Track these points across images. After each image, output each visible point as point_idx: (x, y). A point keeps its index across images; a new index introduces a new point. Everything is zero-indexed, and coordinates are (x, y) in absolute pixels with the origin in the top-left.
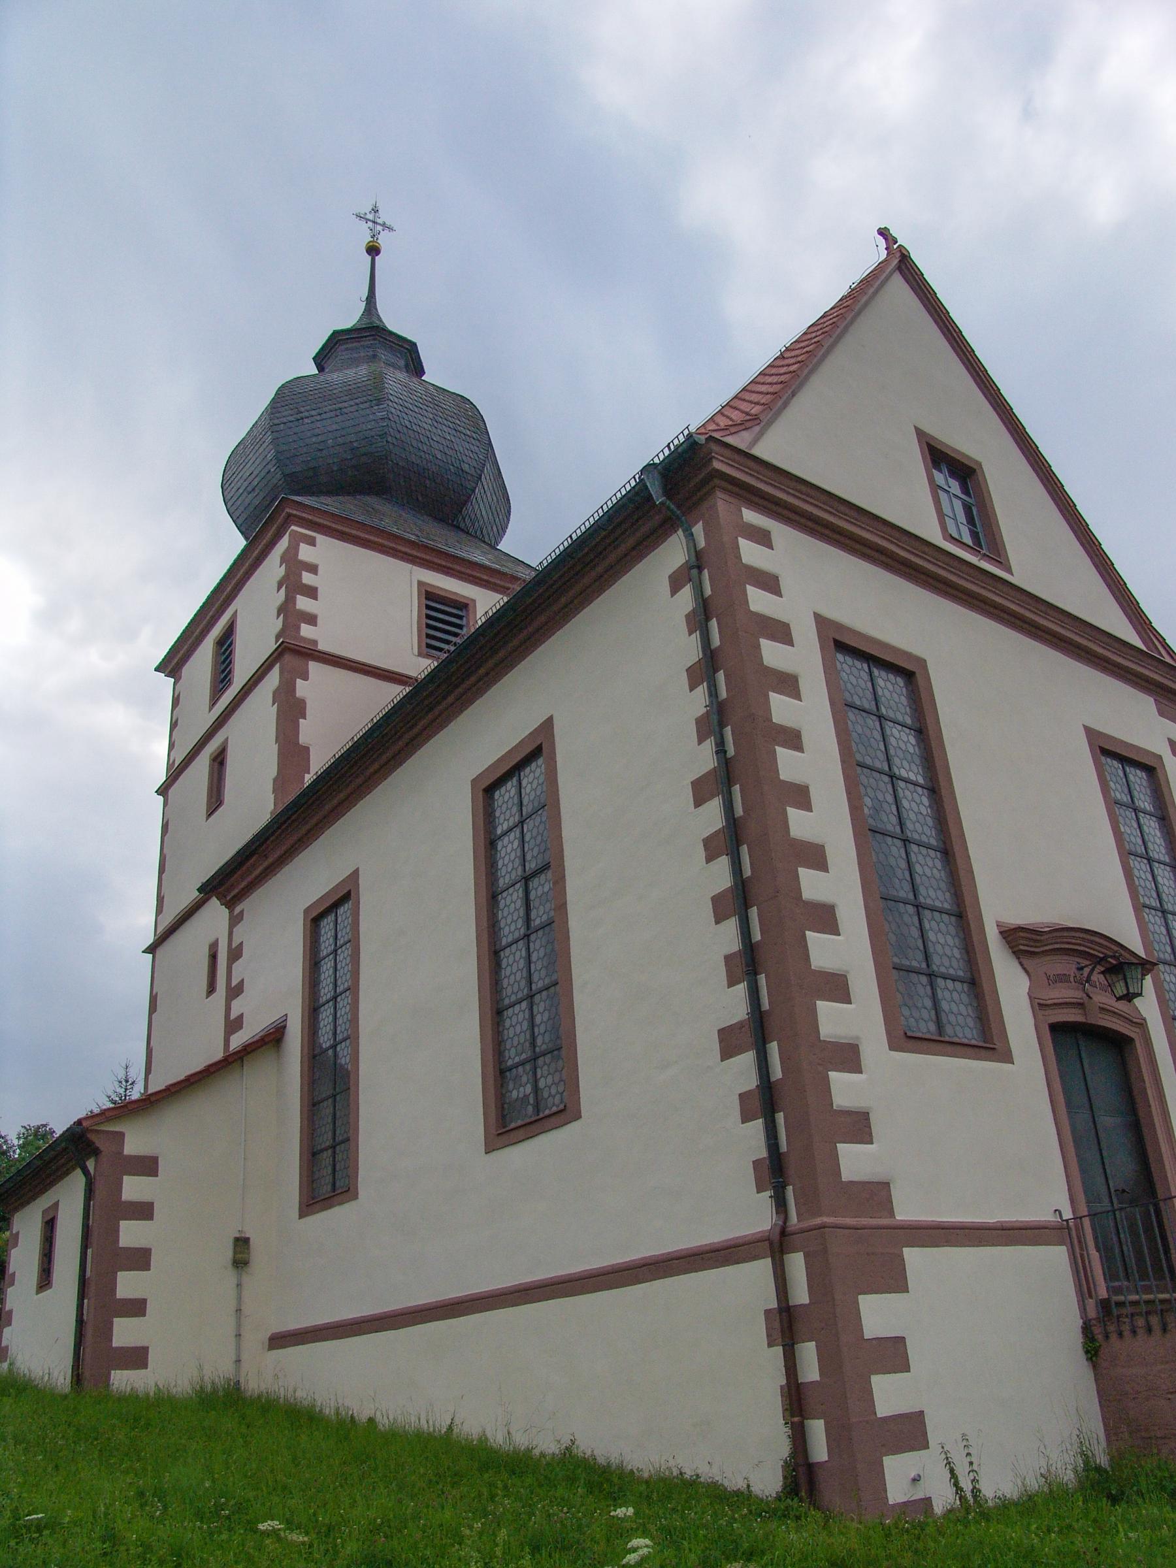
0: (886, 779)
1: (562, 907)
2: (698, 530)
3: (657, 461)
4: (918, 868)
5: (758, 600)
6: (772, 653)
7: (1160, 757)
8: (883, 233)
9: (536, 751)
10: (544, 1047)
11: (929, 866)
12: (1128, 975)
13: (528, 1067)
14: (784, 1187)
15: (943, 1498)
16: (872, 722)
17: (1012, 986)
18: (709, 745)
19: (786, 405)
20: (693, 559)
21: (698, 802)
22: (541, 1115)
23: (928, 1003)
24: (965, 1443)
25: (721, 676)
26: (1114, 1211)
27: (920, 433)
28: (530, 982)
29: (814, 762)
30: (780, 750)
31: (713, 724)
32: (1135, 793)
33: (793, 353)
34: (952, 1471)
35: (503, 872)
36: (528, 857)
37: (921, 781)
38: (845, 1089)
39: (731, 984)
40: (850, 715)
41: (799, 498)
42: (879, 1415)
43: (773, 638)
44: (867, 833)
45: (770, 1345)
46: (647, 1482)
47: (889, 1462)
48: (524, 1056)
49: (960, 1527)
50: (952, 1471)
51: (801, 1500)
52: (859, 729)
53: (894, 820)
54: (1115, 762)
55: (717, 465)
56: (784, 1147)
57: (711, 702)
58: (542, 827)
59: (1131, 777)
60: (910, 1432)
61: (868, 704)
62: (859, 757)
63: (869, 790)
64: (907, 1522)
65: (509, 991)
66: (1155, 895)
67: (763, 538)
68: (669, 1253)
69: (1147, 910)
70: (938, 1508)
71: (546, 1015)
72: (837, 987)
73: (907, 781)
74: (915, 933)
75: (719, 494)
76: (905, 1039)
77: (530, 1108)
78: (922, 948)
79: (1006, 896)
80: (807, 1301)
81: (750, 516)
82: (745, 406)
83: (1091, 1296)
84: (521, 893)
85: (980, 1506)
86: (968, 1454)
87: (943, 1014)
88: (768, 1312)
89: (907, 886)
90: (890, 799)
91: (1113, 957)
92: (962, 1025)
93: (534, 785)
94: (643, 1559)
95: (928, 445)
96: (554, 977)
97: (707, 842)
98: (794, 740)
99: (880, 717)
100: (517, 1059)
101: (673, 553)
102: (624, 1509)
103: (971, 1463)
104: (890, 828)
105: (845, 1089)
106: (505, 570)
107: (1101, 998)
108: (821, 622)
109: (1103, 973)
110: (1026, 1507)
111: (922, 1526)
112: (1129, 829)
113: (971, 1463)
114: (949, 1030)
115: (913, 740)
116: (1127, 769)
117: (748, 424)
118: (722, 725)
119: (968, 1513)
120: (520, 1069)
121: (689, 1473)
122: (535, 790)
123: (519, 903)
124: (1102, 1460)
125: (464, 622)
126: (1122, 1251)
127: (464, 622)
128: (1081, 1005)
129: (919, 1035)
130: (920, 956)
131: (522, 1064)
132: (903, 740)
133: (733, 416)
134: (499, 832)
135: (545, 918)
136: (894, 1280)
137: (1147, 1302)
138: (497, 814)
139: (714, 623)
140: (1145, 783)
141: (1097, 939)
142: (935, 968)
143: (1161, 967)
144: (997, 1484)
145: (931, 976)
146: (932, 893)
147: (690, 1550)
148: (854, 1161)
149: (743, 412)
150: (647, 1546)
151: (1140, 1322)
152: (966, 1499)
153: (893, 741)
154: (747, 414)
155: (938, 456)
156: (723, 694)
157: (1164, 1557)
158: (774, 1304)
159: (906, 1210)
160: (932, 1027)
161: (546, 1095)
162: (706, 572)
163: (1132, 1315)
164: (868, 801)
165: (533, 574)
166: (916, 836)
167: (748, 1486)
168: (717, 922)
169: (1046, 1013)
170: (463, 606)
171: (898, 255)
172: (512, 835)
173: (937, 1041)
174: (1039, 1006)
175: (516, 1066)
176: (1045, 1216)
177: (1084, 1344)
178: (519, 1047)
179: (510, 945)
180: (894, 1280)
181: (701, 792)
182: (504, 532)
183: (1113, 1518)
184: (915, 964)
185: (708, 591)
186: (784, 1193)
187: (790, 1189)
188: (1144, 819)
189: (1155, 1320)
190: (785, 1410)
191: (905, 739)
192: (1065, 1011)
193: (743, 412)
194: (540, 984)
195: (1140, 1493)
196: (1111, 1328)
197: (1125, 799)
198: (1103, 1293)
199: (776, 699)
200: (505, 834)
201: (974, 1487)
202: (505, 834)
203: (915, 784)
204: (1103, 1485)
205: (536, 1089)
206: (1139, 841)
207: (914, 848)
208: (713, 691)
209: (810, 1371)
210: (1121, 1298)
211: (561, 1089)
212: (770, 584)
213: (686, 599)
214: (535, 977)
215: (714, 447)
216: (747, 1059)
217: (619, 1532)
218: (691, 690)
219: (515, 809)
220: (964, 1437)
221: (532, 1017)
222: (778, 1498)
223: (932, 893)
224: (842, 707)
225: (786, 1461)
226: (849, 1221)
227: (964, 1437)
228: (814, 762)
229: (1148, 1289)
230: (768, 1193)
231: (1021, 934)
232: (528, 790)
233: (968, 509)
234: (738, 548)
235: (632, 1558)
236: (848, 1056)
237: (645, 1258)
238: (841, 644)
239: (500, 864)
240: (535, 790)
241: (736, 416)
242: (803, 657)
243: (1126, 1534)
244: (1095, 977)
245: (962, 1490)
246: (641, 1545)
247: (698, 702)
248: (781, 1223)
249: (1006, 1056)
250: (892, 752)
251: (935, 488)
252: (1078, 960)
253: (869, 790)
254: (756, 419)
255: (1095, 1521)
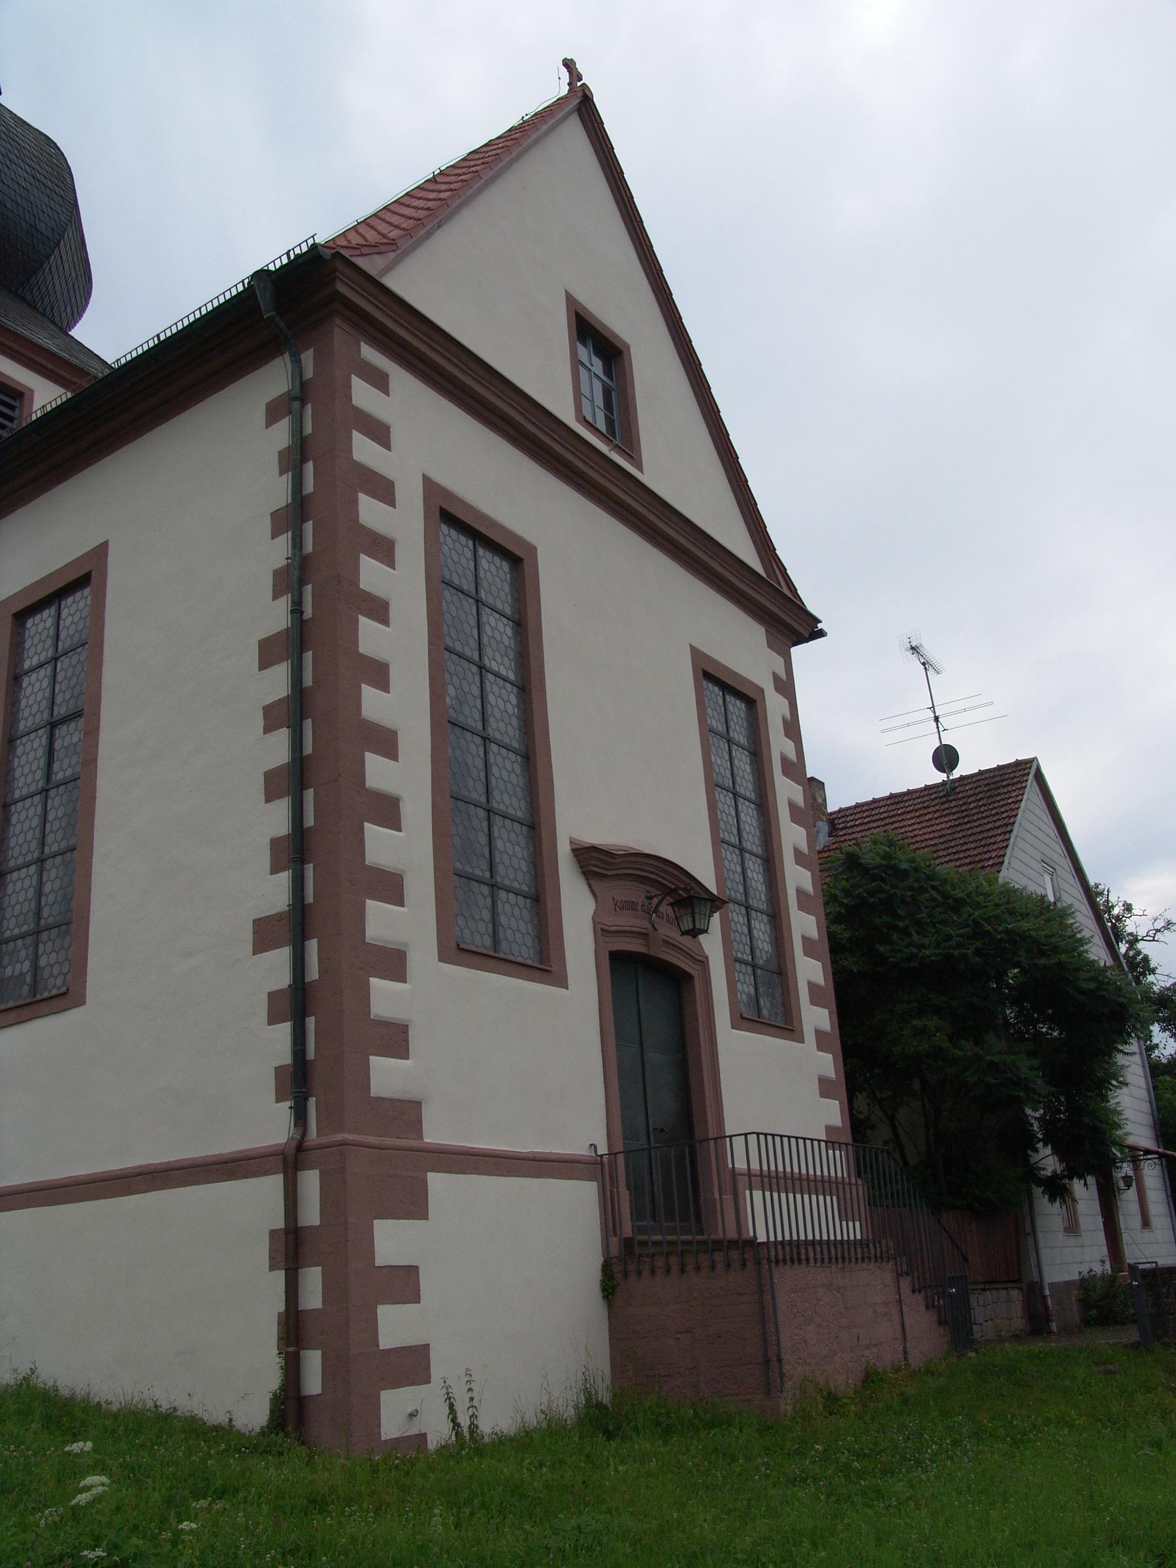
0: (475, 669)
1: (91, 762)
2: (308, 357)
3: (272, 268)
4: (495, 770)
5: (364, 449)
6: (370, 511)
7: (762, 691)
8: (569, 64)
9: (82, 579)
10: (51, 920)
11: (507, 769)
12: (697, 910)
13: (29, 940)
14: (306, 1099)
15: (438, 1432)
16: (470, 606)
17: (577, 907)
18: (284, 604)
19: (429, 235)
20: (297, 389)
21: (264, 664)
22: (38, 997)
23: (486, 915)
24: (468, 1378)
25: (309, 527)
26: (649, 1150)
27: (570, 300)
28: (43, 844)
29: (399, 639)
30: (363, 620)
31: (293, 579)
32: (732, 724)
33: (447, 179)
34: (451, 1407)
35: (26, 713)
36: (59, 699)
37: (512, 676)
38: (386, 997)
39: (275, 870)
40: (446, 592)
41: (425, 343)
42: (381, 1347)
43: (373, 494)
44: (445, 724)
45: (272, 1267)
46: (116, 1416)
47: (387, 1397)
48: (25, 928)
49: (452, 1463)
50: (451, 1407)
51: (287, 1435)
52: (454, 612)
53: (477, 715)
54: (716, 689)
55: (341, 288)
56: (311, 1054)
57: (294, 554)
58: (78, 669)
59: (730, 707)
60: (412, 1365)
61: (468, 586)
62: (449, 642)
63: (455, 679)
64: (397, 1458)
65: (16, 852)
66: (735, 832)
67: (380, 381)
68: (169, 1163)
69: (726, 846)
70: (432, 1444)
71: (57, 883)
72: (391, 887)
73: (497, 675)
74: (483, 840)
75: (338, 321)
76: (456, 951)
77: (26, 989)
78: (487, 856)
79: (587, 812)
80: (316, 1222)
81: (369, 353)
82: (383, 227)
83: (615, 1234)
84: (44, 741)
85: (476, 1442)
86: (470, 1390)
87: (501, 930)
88: (273, 1233)
89: (481, 788)
90: (476, 691)
91: (684, 890)
92: (521, 945)
93: (76, 619)
94: (98, 1499)
95: (578, 315)
96: (72, 842)
97: (268, 711)
98: (379, 610)
99: (478, 601)
100: (16, 931)
101: (273, 380)
102: (81, 1444)
103: (472, 1399)
104: (471, 722)
105: (386, 997)
106: (76, 362)
107: (668, 931)
108: (429, 485)
109: (672, 905)
110: (522, 1443)
111: (413, 1463)
112: (720, 761)
113: (472, 1399)
114: (504, 946)
115: (509, 632)
116: (728, 697)
117: (383, 249)
118: (302, 582)
119: (462, 1449)
120: (20, 942)
121: (165, 1406)
122: (76, 624)
123: (40, 752)
124: (605, 1397)
125: (16, 414)
126: (653, 1191)
127: (16, 414)
128: (644, 936)
129: (474, 948)
130: (485, 865)
131: (23, 936)
132: (499, 631)
133: (368, 236)
134: (27, 665)
135: (69, 772)
136: (414, 1206)
137: (670, 1243)
138: (27, 645)
139: (309, 467)
140: (743, 714)
141: (672, 870)
142: (499, 879)
143: (731, 905)
144: (496, 1419)
145: (494, 887)
146: (506, 799)
147: (154, 1489)
148: (387, 1076)
149: (379, 233)
150: (103, 1484)
151: (660, 1262)
152: (462, 1434)
153: (488, 629)
154: (384, 236)
155: (586, 330)
156: (309, 547)
157: (647, 1487)
158: (280, 1224)
159: (436, 1133)
160: (488, 941)
161: (46, 974)
162: (309, 409)
163: (653, 1255)
164: (451, 690)
165: (107, 372)
166: (498, 736)
167: (231, 1420)
168: (268, 800)
169: (607, 939)
170: (16, 395)
171: (580, 94)
172: (42, 672)
173: (490, 957)
174: (601, 931)
175: (15, 939)
176: (579, 1149)
177: (603, 1281)
178: (21, 918)
179: (23, 799)
180: (414, 1206)
181: (268, 654)
182: (80, 316)
183: (605, 1453)
184: (478, 872)
185: (308, 429)
186: (305, 1105)
187: (312, 1101)
188: (737, 753)
189: (674, 1260)
190: (280, 1339)
191: (502, 630)
192: (627, 939)
193: (379, 233)
194: (55, 848)
195: (636, 1430)
196: (631, 1267)
197: (721, 728)
198: (628, 1231)
199: (367, 563)
200: (33, 669)
201: (472, 1423)
202: (33, 669)
203: (505, 680)
204: (600, 1420)
205: (35, 967)
206: (728, 773)
207: (494, 747)
208: (298, 543)
209: (313, 1296)
210: (644, 1238)
211: (65, 970)
212: (380, 433)
213: (281, 434)
214: (50, 839)
215: (339, 265)
216: (282, 956)
217: (73, 1470)
218: (273, 538)
219: (49, 642)
220: (468, 1373)
221: (41, 884)
222: (262, 1433)
223: (506, 799)
224: (439, 584)
225: (275, 1394)
226: (373, 1140)
227: (468, 1373)
228: (399, 639)
229: (673, 1231)
230: (288, 1104)
231: (594, 854)
232: (68, 622)
233: (607, 393)
234: (349, 387)
235: (83, 1498)
236: (393, 964)
237: (141, 1167)
238: (449, 515)
239: (23, 704)
240: (76, 624)
241: (372, 237)
242: (403, 521)
243: (616, 1468)
244: (662, 909)
245: (459, 1425)
246: (97, 1482)
247: (279, 551)
248: (298, 1137)
249: (561, 981)
250: (485, 640)
251: (576, 363)
252: (650, 889)
253: (455, 679)
254: (392, 244)
255: (588, 1456)
